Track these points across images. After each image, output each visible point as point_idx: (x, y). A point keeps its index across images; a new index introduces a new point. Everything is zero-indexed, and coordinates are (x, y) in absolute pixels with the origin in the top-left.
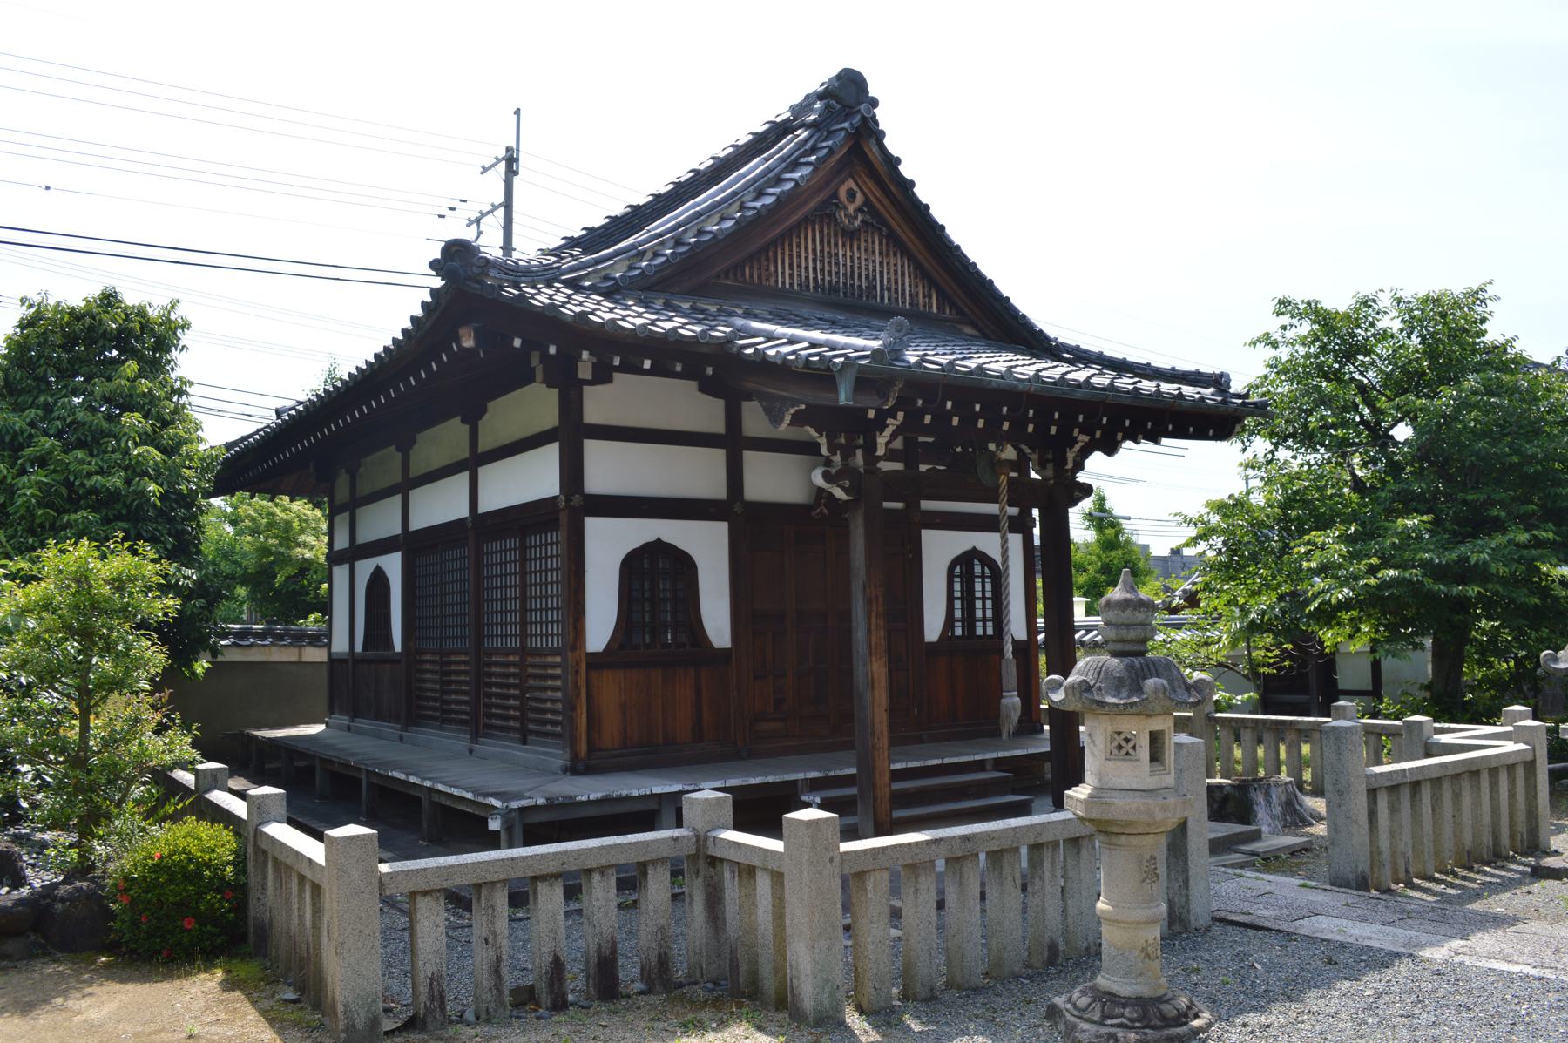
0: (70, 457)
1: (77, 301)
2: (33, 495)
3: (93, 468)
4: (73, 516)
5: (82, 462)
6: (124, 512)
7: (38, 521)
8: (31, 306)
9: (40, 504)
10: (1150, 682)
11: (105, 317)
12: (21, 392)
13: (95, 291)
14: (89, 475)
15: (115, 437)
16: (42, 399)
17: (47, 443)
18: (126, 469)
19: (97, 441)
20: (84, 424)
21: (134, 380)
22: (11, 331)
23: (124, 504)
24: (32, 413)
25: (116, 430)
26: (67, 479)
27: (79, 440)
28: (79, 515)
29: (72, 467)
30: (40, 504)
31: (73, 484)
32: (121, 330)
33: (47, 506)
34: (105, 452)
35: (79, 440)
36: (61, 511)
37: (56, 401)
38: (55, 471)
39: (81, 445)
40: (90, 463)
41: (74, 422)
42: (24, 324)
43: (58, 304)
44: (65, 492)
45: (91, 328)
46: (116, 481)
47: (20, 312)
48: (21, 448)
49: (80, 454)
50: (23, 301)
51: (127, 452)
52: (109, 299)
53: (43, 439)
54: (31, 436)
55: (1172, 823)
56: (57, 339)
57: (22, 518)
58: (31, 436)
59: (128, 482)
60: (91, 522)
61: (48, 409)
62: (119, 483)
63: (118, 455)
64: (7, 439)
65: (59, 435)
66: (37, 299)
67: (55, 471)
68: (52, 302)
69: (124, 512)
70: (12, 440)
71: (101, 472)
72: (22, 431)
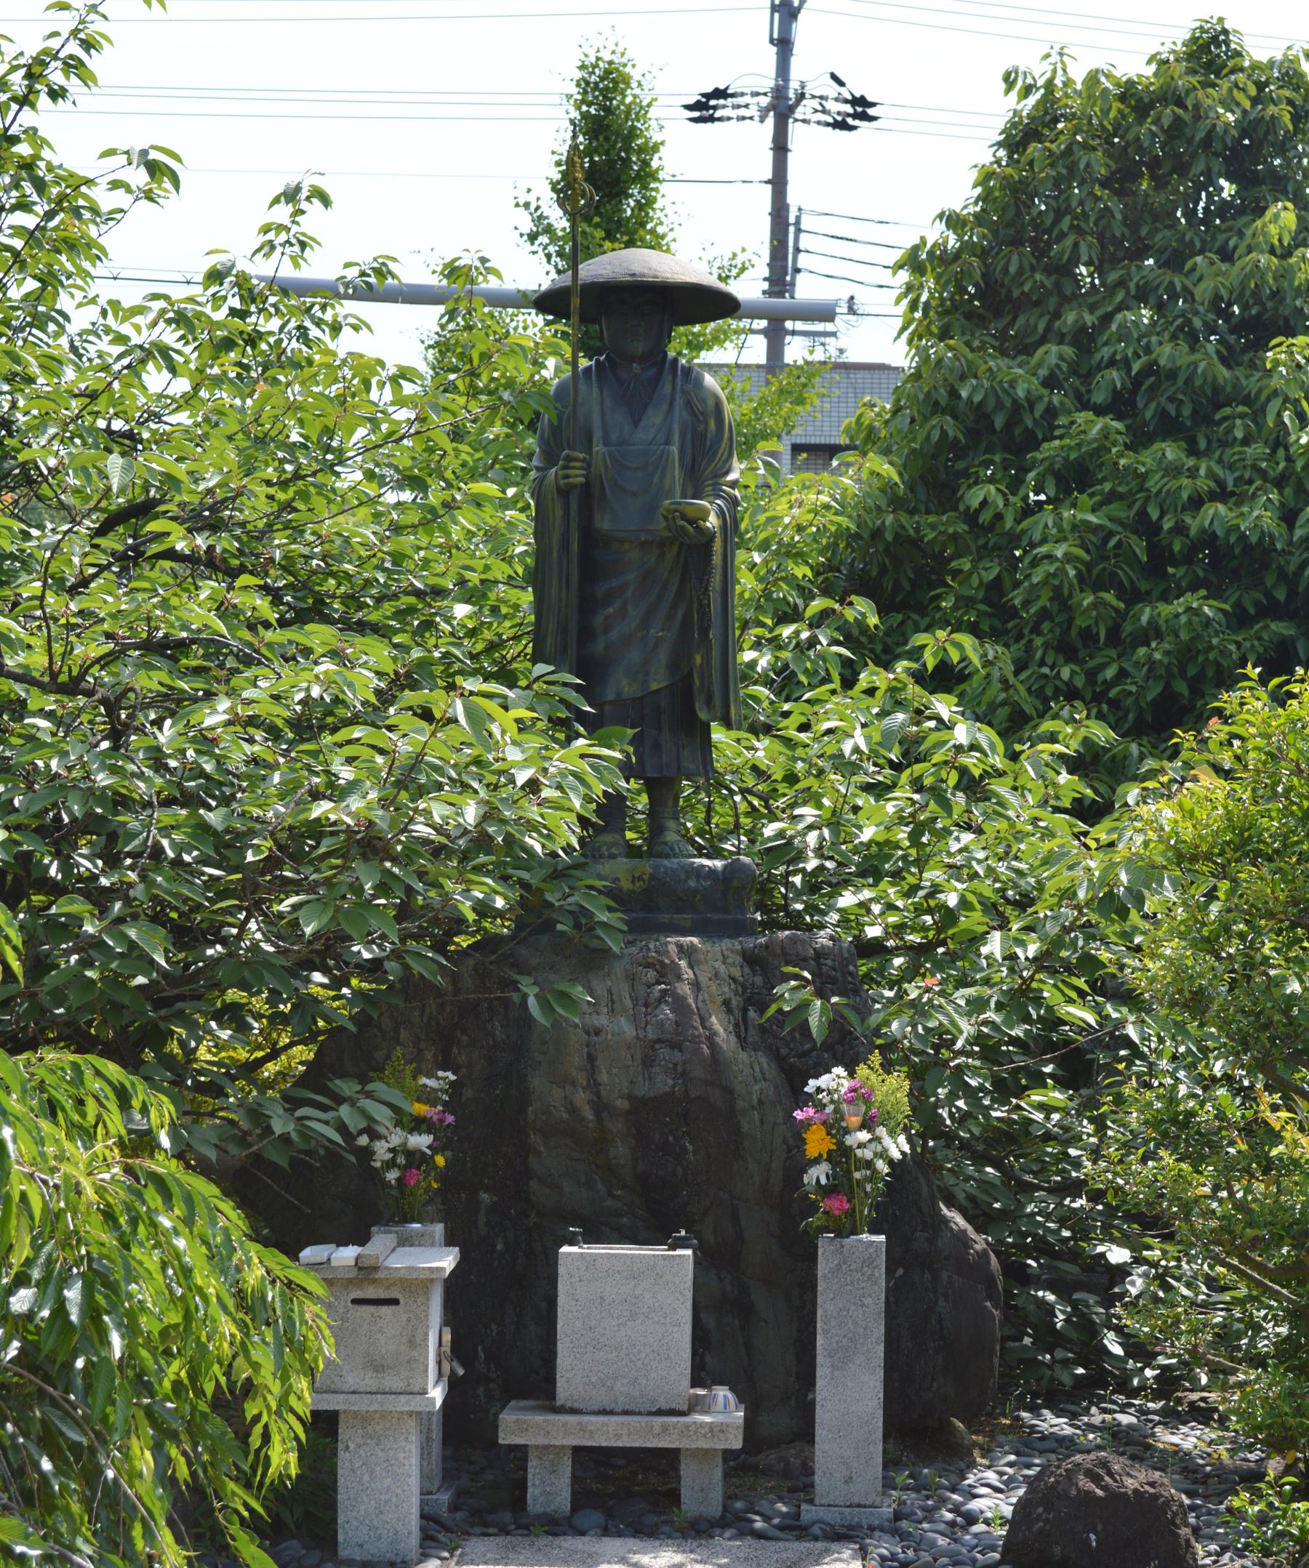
0: (1146, 460)
1: (1133, 64)
2: (1068, 558)
3: (1204, 484)
4: (1165, 609)
5: (1174, 471)
6: (1281, 595)
7: (1081, 622)
8: (1027, 91)
9: (1089, 580)
10: (1150, 1163)
11: (1208, 98)
12: (1019, 305)
13: (1174, 35)
14: (1196, 503)
15: (1247, 401)
16: (1070, 317)
17: (1094, 426)
18: (1279, 483)
19: (1204, 417)
20: (1172, 374)
21: (1287, 253)
22: (986, 157)
23: (1282, 575)
24: (1052, 354)
25: (1251, 383)
26: (1143, 513)
27: (1162, 414)
28: (1179, 605)
29: (1153, 484)
30: (1089, 580)
31: (1157, 527)
32: (1247, 127)
33: (1097, 586)
34: (1226, 443)
35: (1162, 414)
36: (1133, 597)
37: (1108, 318)
38: (1111, 497)
39: (1168, 427)
40: (1193, 473)
41: (1150, 369)
42: (1019, 138)
43: (1093, 78)
44: (1140, 547)
45: (1176, 130)
46: (1260, 516)
47: (1001, 109)
48: (1033, 443)
49: (1172, 451)
50: (1009, 80)
51: (1279, 441)
52: (1210, 52)
53: (1082, 417)
54: (1051, 412)
55: (846, 297)
56: (1100, 164)
57: (1044, 614)
58: (1051, 412)
59: (1289, 517)
60: (1207, 622)
61: (1083, 339)
62: (1269, 520)
63: (1257, 449)
64: (999, 422)
65: (1119, 405)
66: (1041, 72)
67: (1111, 497)
68: (1078, 75)
69: (1281, 595)
70: (1009, 426)
71: (1220, 494)
72: (1031, 402)
